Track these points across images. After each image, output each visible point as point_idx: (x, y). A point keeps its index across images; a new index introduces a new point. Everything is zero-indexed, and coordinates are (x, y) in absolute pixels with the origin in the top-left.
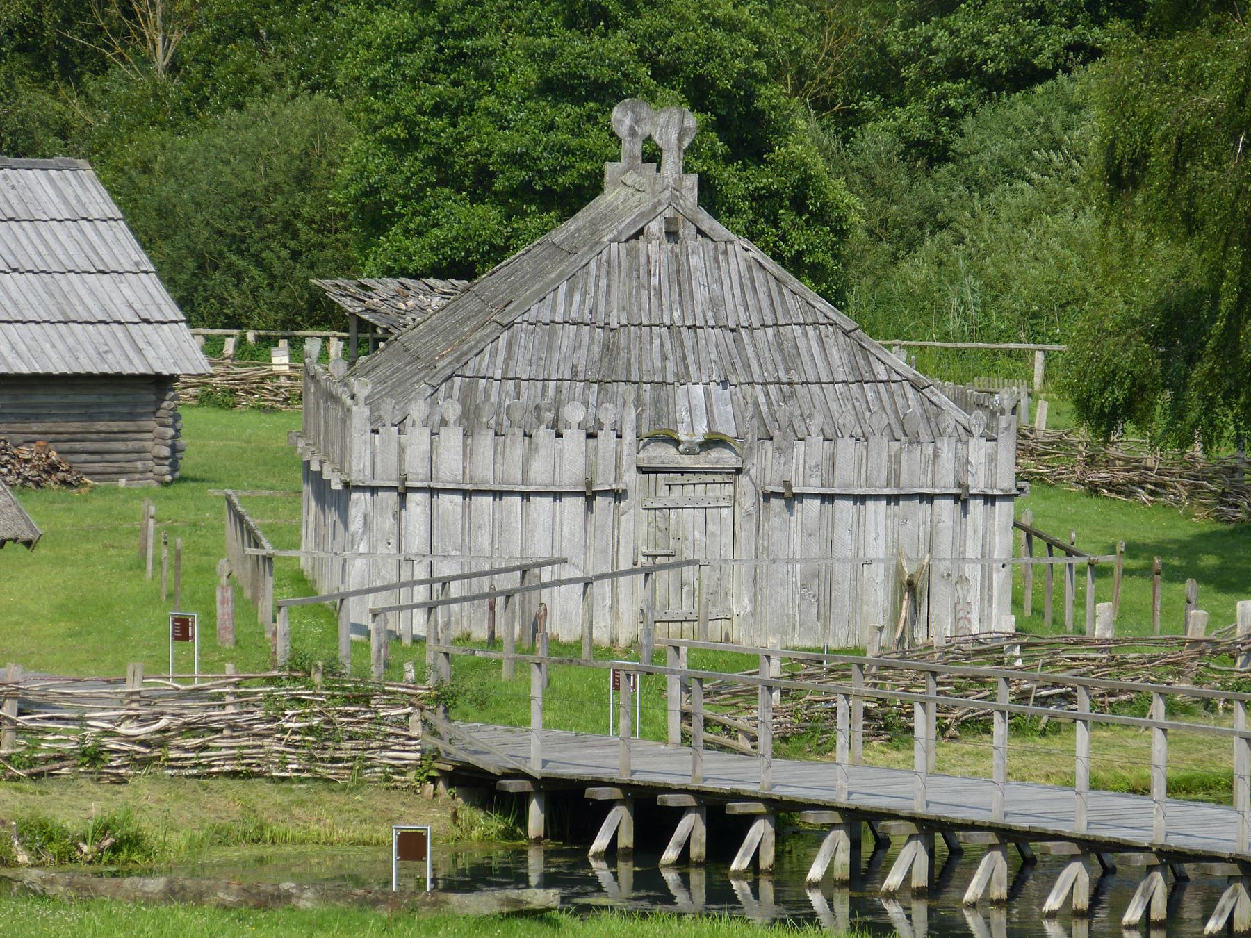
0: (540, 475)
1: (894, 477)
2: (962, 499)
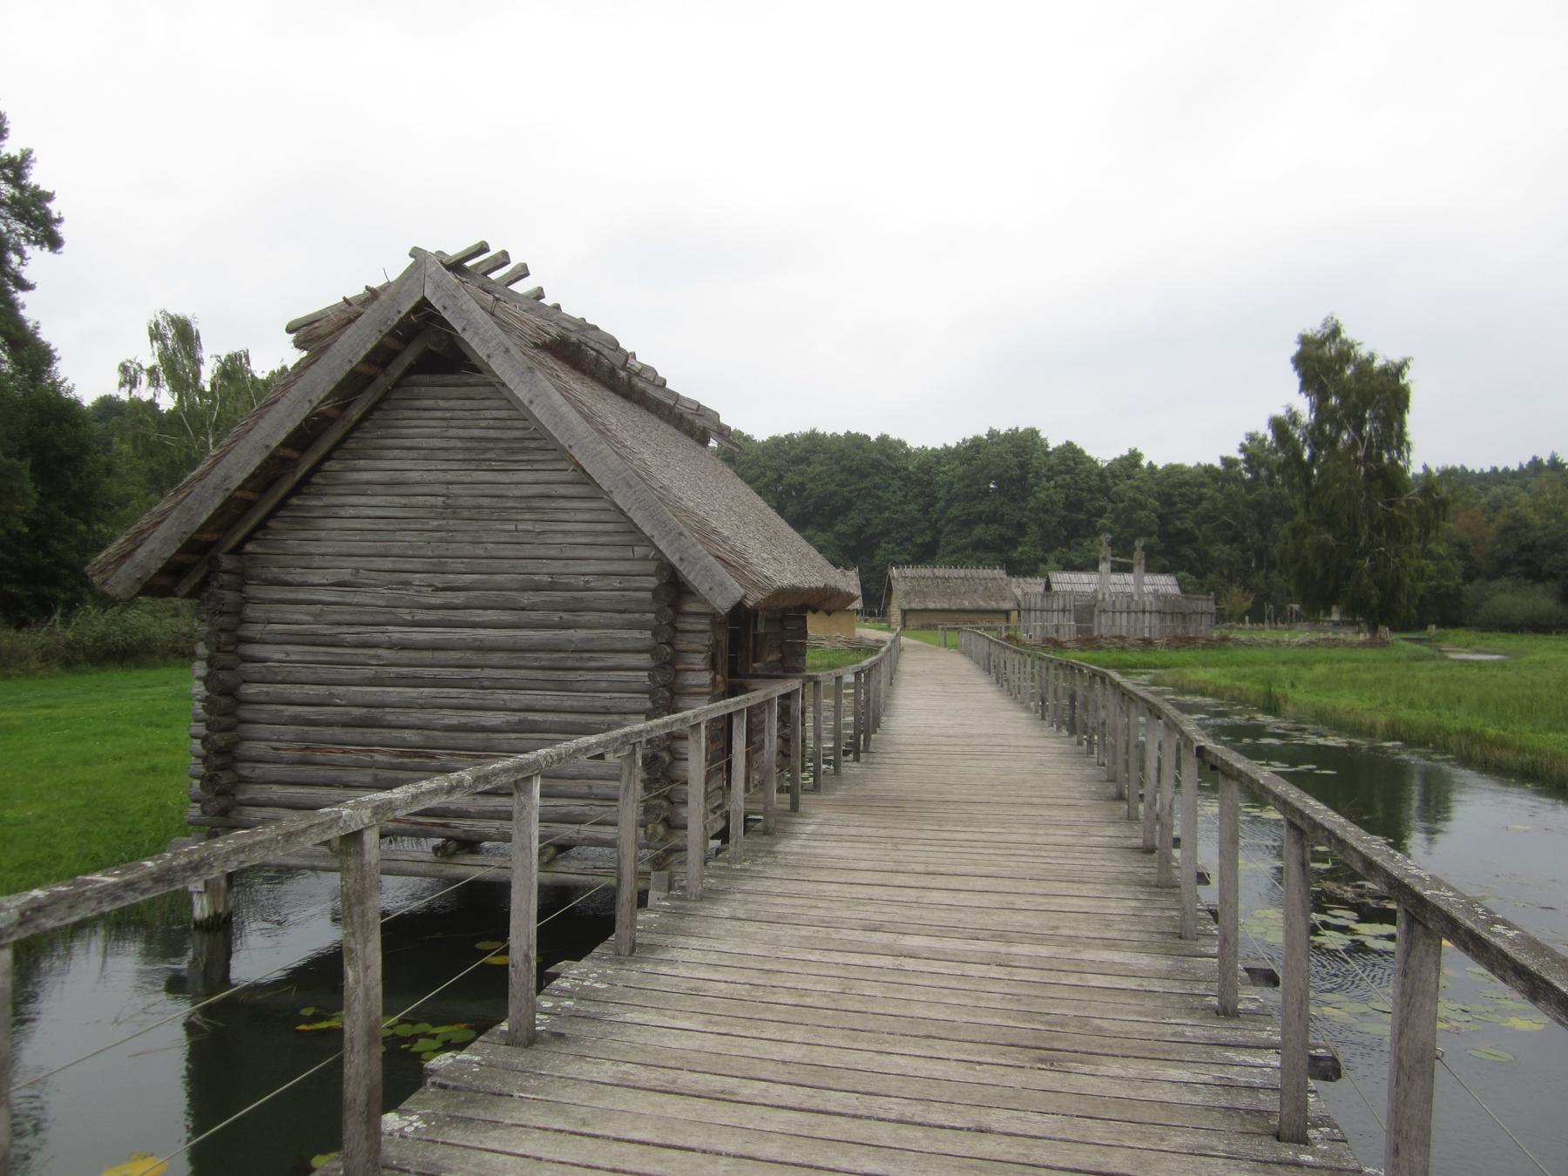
0: (1055, 607)
1: (1128, 607)
2: (1128, 612)
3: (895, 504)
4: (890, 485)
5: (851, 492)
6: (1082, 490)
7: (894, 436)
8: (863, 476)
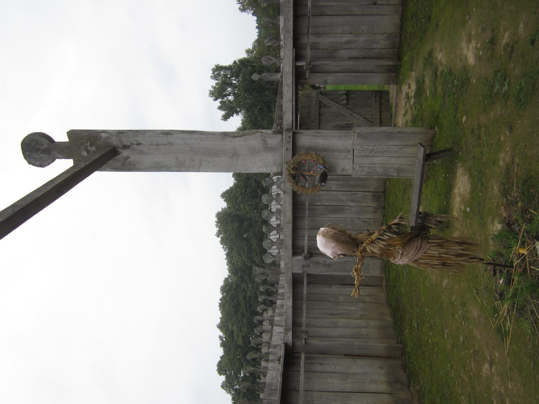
3: (253, 287)
4: (244, 290)
5: (247, 311)
6: (246, 191)
7: (222, 283)
8: (240, 304)
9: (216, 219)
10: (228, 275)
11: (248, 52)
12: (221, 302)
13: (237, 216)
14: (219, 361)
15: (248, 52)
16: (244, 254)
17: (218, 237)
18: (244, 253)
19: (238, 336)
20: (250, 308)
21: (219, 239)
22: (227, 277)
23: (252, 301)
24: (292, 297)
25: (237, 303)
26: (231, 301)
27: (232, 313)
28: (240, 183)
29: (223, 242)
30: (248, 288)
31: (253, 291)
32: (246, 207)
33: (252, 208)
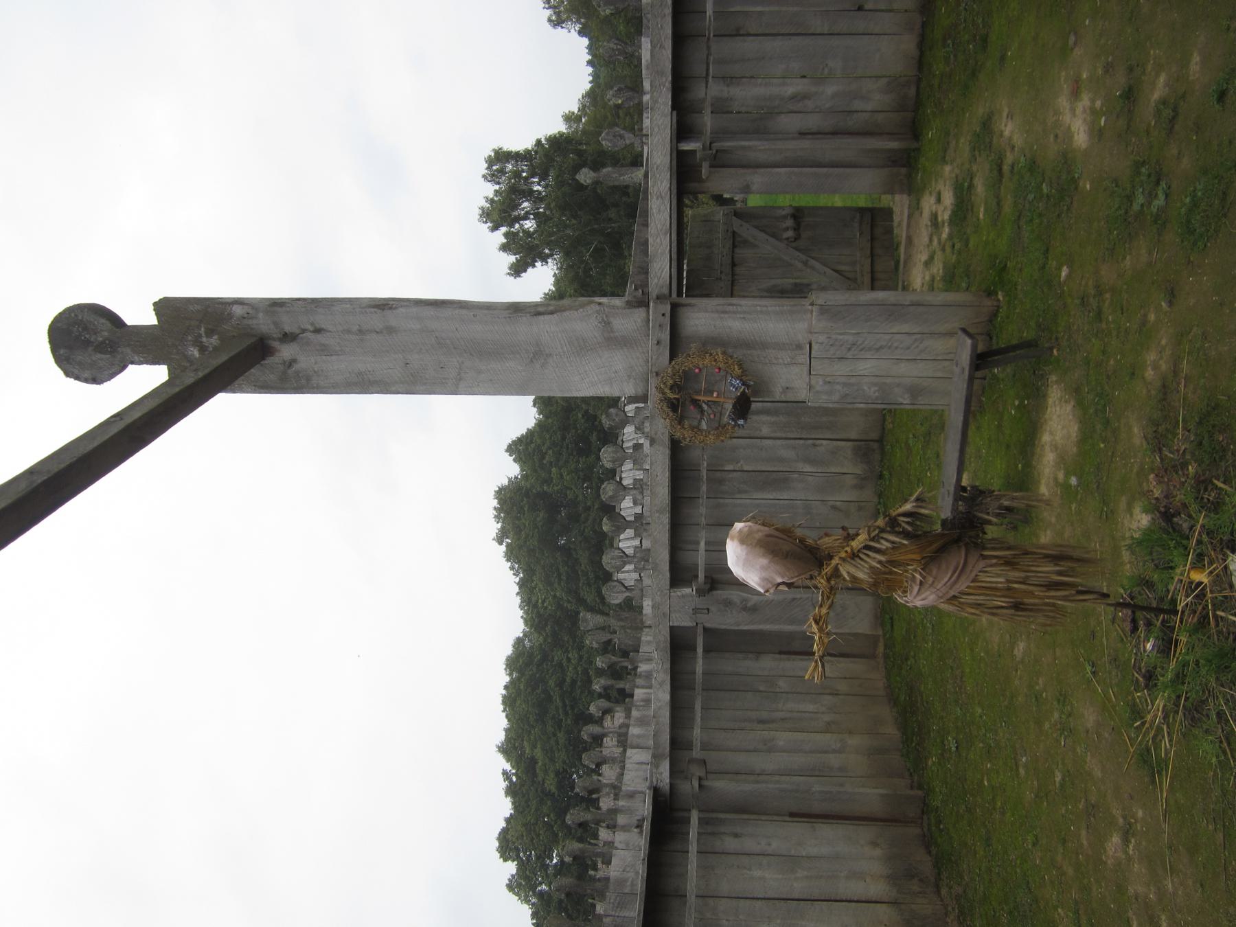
3: (581, 658)
4: (560, 665)
5: (566, 714)
6: (564, 438)
7: (508, 650)
8: (549, 699)
9: (495, 503)
10: (524, 632)
11: (568, 118)
12: (508, 693)
13: (543, 496)
14: (503, 828)
15: (568, 118)
16: (559, 584)
17: (501, 543)
18: (560, 580)
19: (546, 772)
20: (572, 708)
21: (503, 548)
22: (521, 635)
23: (578, 691)
24: (669, 681)
25: (543, 696)
26: (529, 690)
27: (532, 719)
28: (550, 420)
29: (510, 555)
30: (569, 660)
31: (579, 669)
32: (565, 475)
33: (579, 478)
